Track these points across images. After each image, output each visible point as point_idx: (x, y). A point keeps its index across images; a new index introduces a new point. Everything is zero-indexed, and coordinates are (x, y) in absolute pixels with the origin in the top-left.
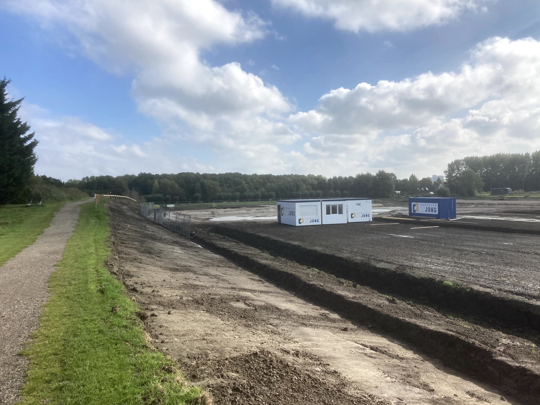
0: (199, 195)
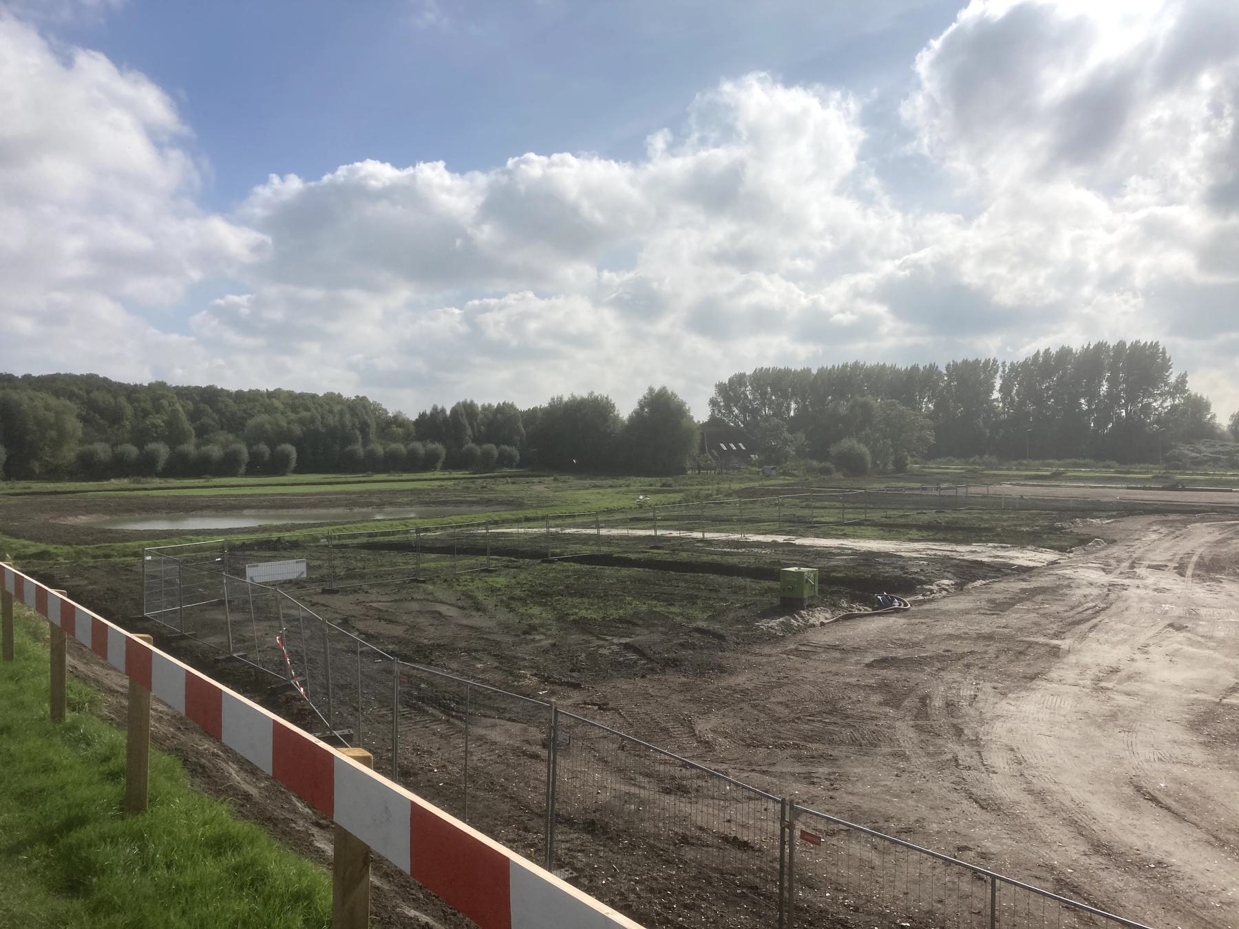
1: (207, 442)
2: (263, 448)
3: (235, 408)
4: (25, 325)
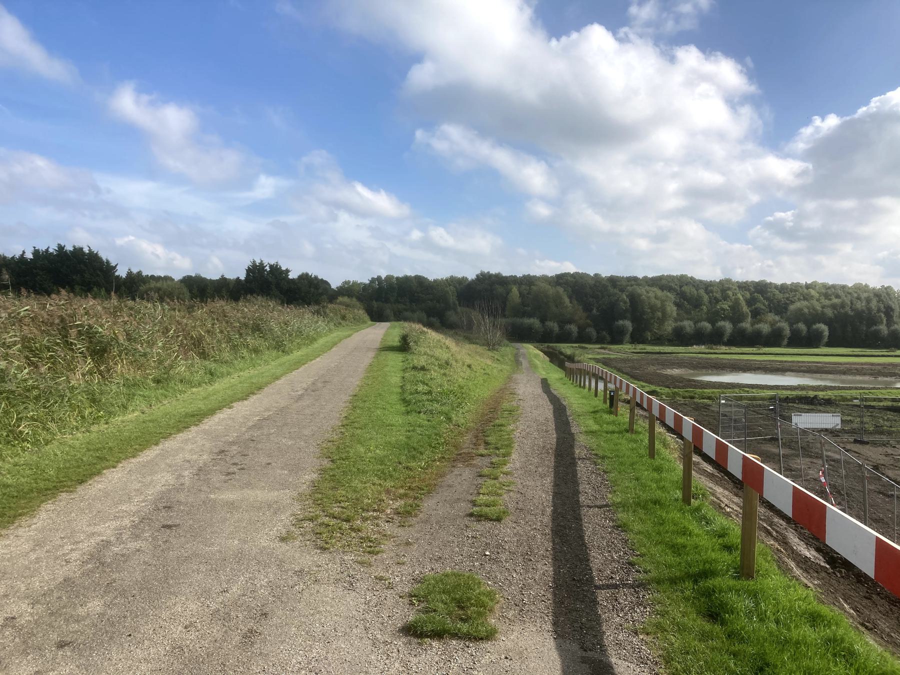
0: (628, 324)
1: (760, 321)
2: (802, 326)
3: (780, 296)
4: (643, 244)
